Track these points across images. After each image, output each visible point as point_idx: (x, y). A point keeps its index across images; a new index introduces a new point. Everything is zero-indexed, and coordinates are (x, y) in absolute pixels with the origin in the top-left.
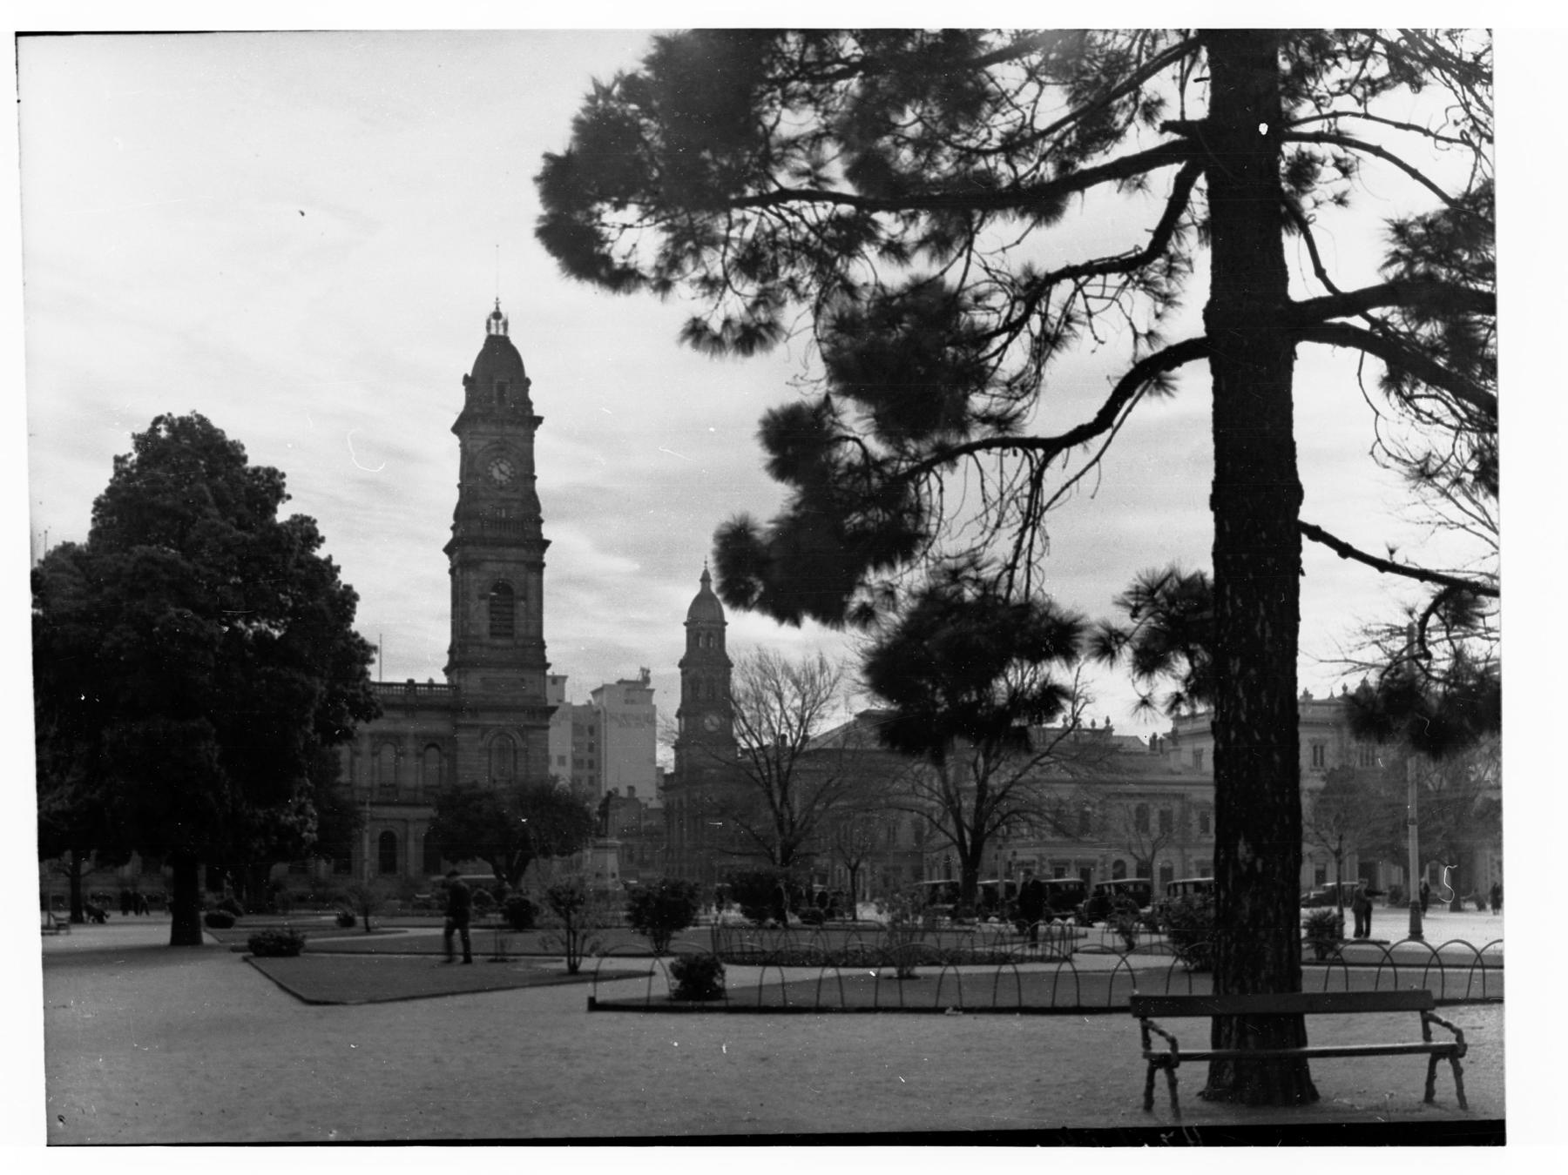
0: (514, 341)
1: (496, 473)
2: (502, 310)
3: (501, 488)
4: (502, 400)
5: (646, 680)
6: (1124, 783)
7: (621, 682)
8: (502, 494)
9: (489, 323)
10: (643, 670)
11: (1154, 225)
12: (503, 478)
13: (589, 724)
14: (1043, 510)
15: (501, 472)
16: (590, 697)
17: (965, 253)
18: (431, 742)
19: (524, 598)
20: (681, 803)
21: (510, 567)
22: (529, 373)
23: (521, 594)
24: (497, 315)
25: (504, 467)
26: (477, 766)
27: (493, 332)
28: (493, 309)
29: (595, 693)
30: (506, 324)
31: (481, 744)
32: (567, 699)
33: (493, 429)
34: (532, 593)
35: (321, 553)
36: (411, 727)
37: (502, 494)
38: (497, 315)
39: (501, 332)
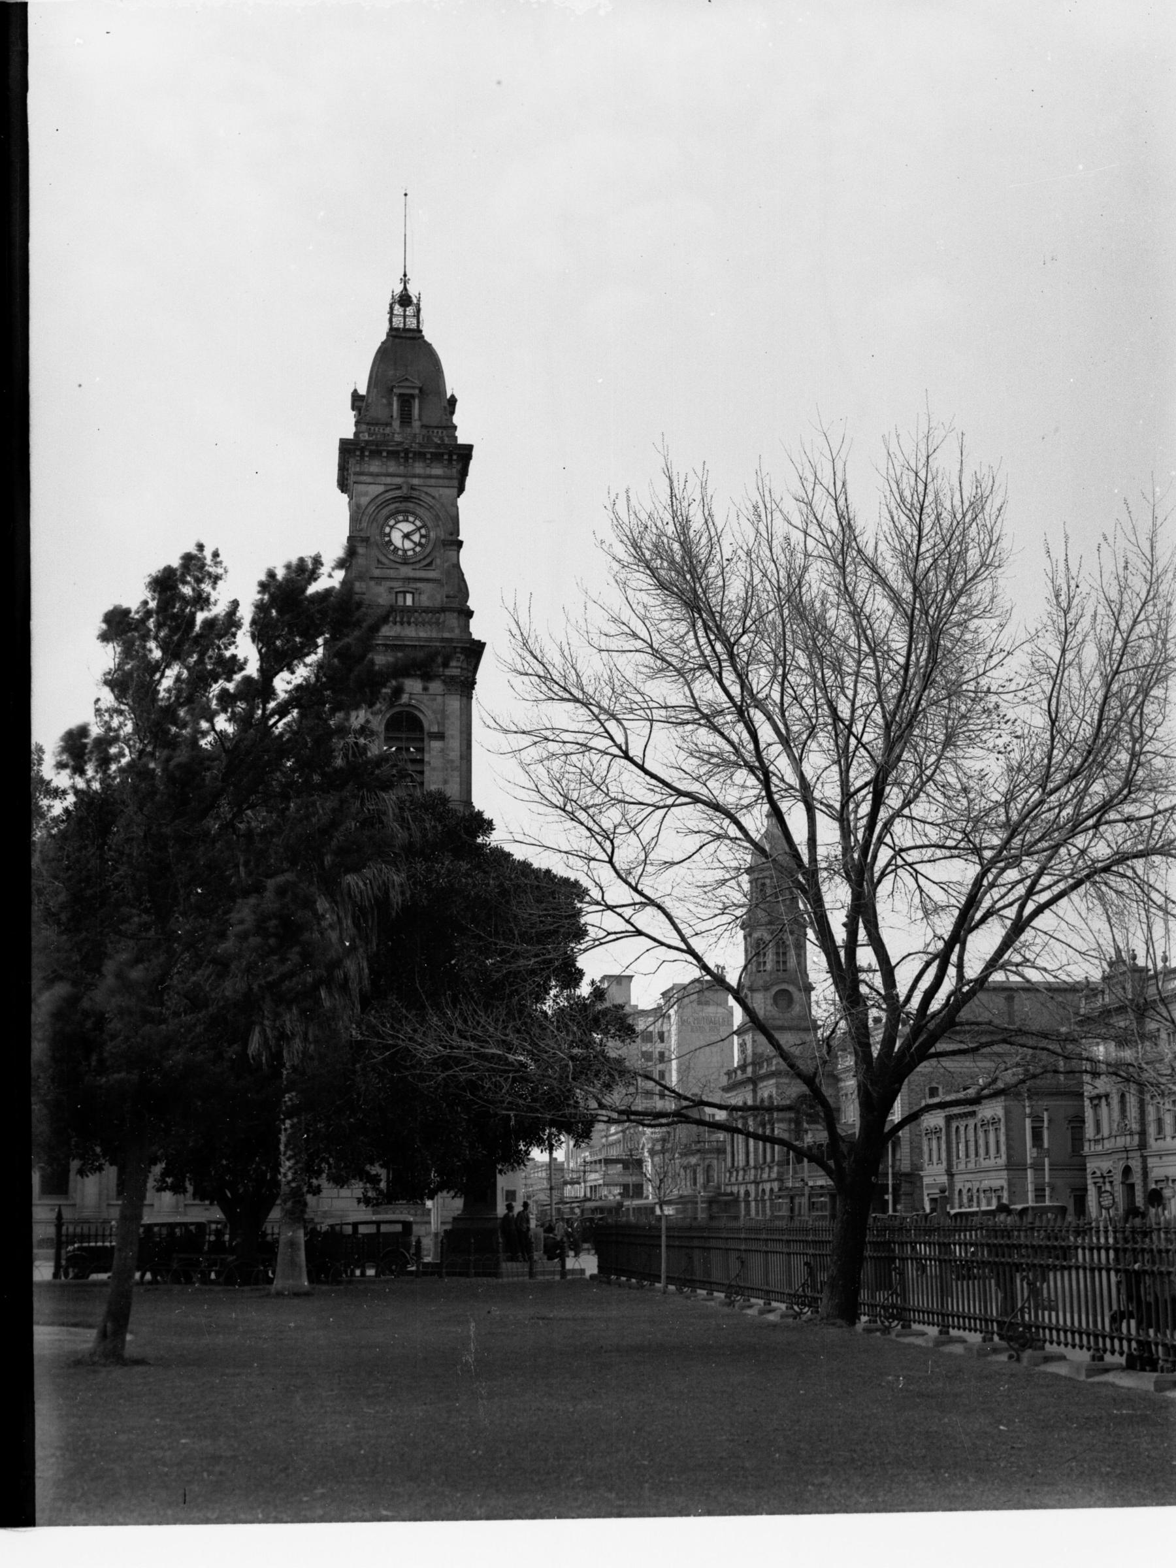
0: (429, 335)
1: (397, 538)
2: (413, 292)
3: (405, 561)
4: (406, 419)
6: (958, 1144)
7: (343, 485)
8: (406, 571)
11: (988, 957)
12: (408, 545)
14: (1028, 981)
17: (1054, 715)
19: (440, 736)
22: (453, 384)
23: (435, 729)
24: (404, 300)
27: (398, 322)
28: (399, 289)
32: (633, 1002)
33: (392, 468)
34: (453, 730)
35: (104, 626)
37: (406, 571)
38: (404, 300)
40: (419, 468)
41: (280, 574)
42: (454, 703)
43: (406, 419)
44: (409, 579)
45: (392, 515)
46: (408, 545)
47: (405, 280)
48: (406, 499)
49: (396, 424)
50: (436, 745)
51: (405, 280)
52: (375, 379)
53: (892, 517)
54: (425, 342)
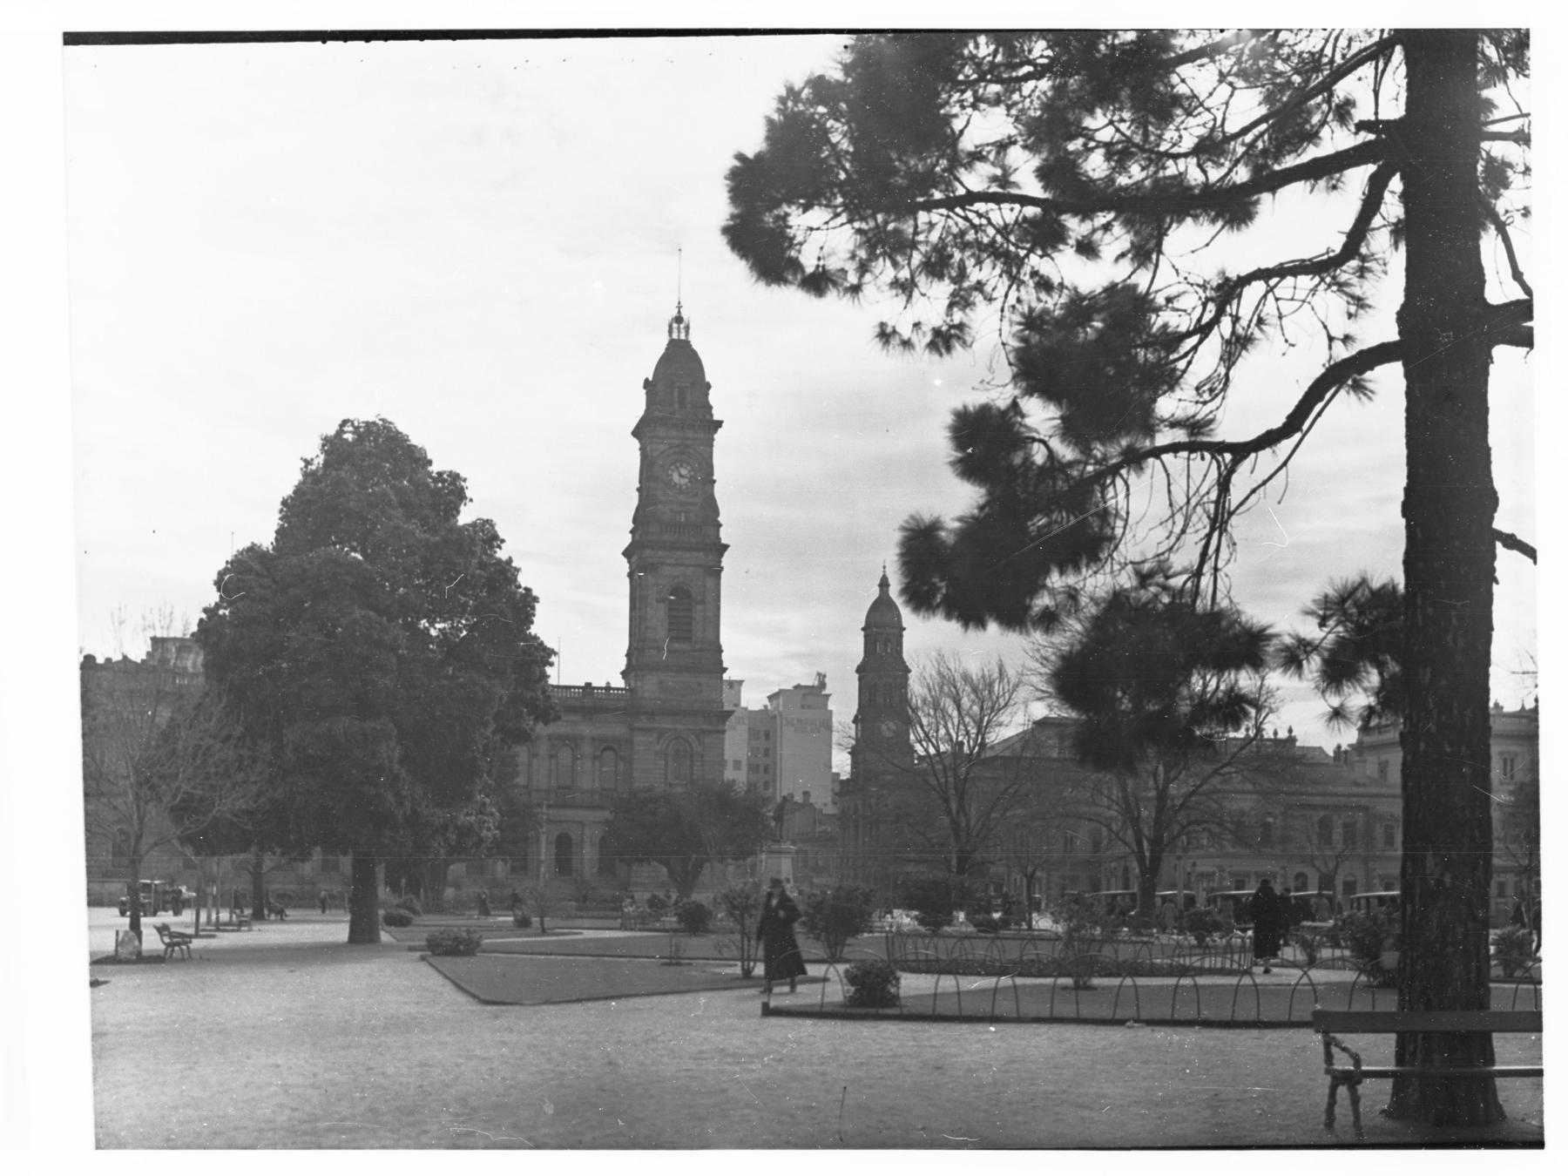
0: (695, 346)
1: (676, 478)
2: (684, 314)
4: (682, 404)
5: (823, 685)
7: (797, 687)
9: (670, 326)
10: (819, 674)
12: (683, 481)
13: (765, 726)
15: (681, 476)
16: (767, 702)
18: (607, 745)
19: (702, 602)
20: (856, 808)
21: (690, 571)
22: (709, 377)
25: (684, 472)
26: (651, 769)
27: (675, 336)
28: (675, 313)
29: (770, 698)
30: (687, 328)
31: (658, 748)
32: (743, 704)
35: (502, 554)
36: (587, 730)
37: (682, 498)
38: (679, 319)
39: (683, 337)
40: (690, 434)
41: (775, 117)
42: (710, 583)
43: (682, 404)
44: (682, 504)
45: (674, 463)
46: (683, 481)
47: (679, 307)
48: (682, 453)
49: (677, 406)
50: (699, 607)
51: (679, 307)
52: (533, 608)
53: (1128, 495)
54: (1407, 296)
